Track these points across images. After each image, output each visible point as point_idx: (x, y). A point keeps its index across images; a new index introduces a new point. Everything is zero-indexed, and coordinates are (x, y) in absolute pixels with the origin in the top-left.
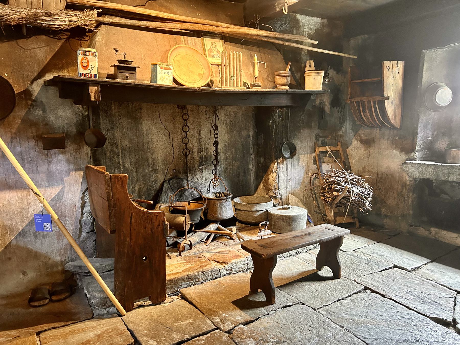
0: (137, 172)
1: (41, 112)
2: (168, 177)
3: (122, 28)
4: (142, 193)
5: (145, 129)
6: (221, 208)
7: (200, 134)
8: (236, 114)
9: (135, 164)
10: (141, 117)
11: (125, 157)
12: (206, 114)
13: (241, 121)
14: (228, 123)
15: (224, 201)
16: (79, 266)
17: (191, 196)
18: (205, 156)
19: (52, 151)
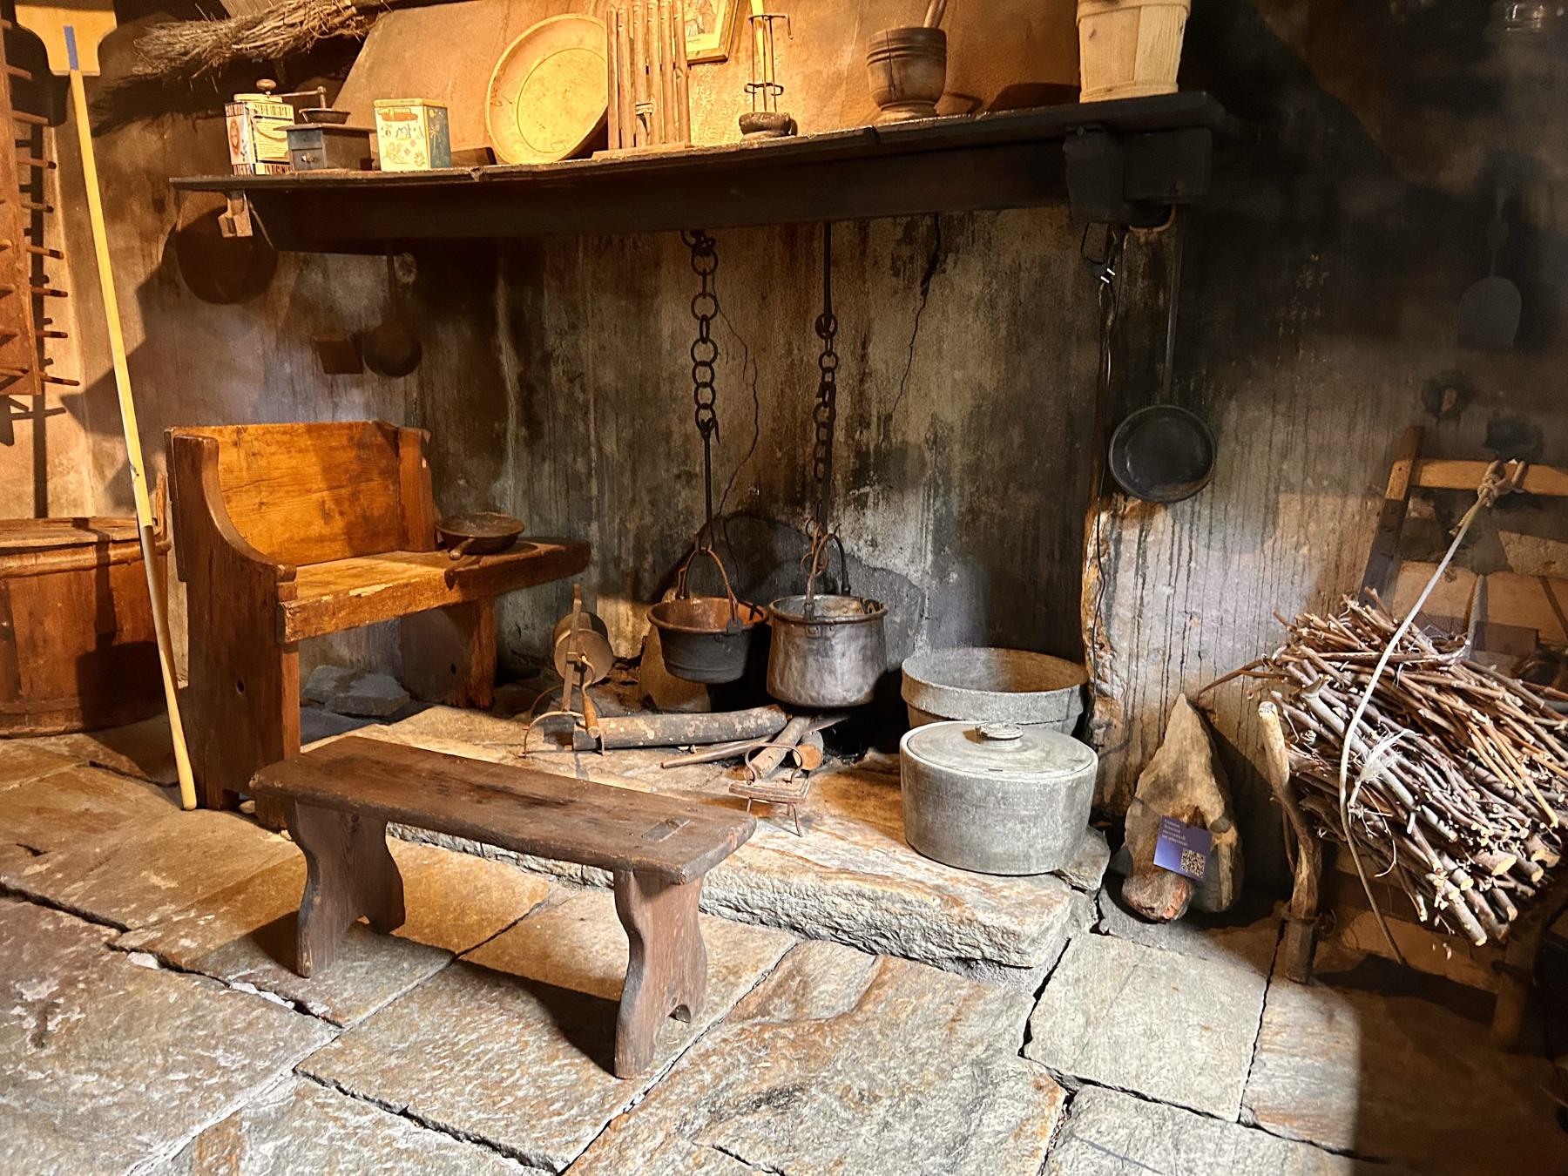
0: (634, 472)
1: (320, 279)
2: (732, 509)
3: (426, 9)
4: (647, 546)
5: (666, 332)
7: (864, 357)
8: (1045, 267)
9: (631, 447)
10: (656, 292)
11: (603, 421)
12: (896, 274)
13: (1069, 299)
14: (1002, 310)
16: (732, 758)
18: (877, 447)
19: (341, 378)
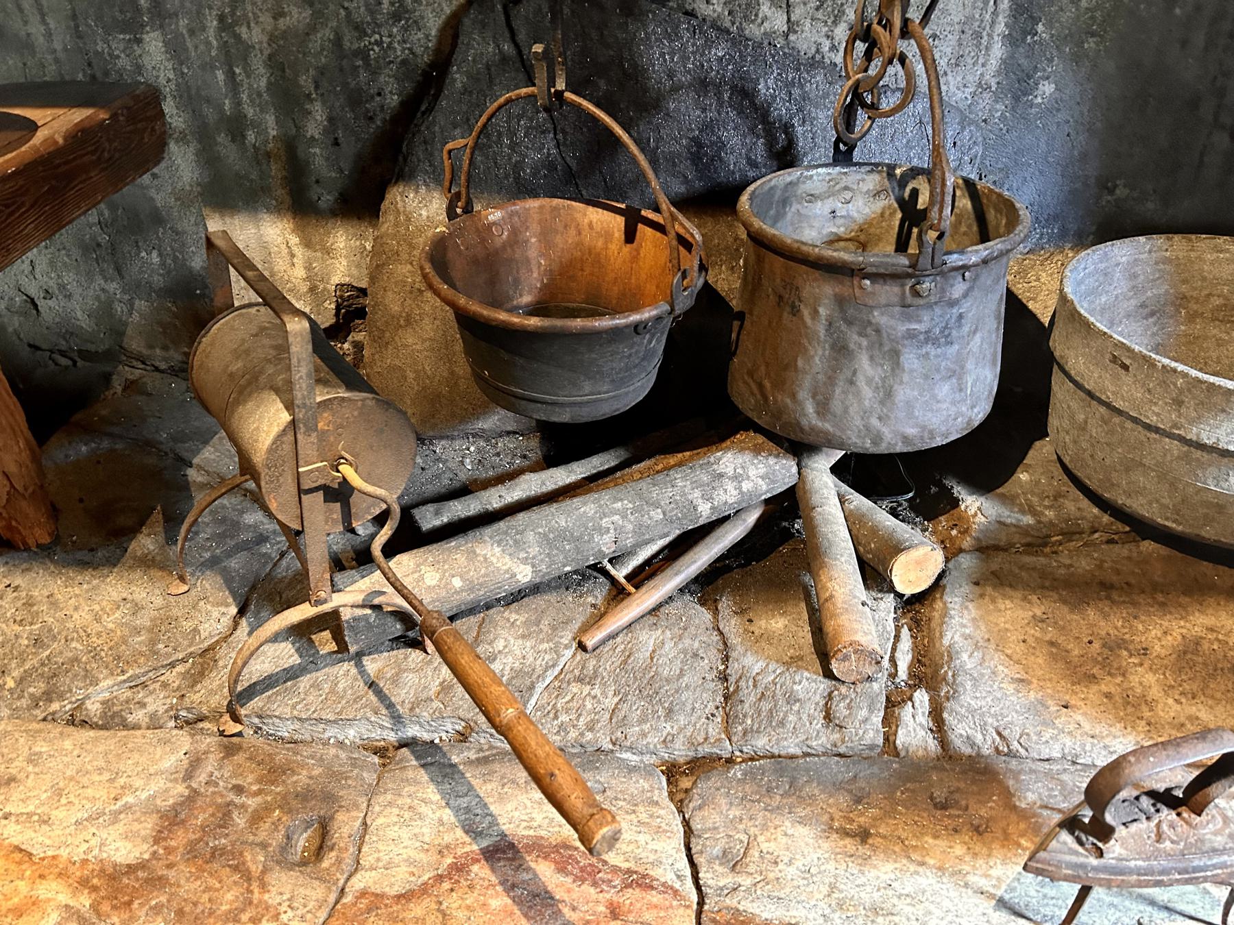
4: (305, 81)
6: (841, 350)
15: (889, 292)
17: (696, 158)
